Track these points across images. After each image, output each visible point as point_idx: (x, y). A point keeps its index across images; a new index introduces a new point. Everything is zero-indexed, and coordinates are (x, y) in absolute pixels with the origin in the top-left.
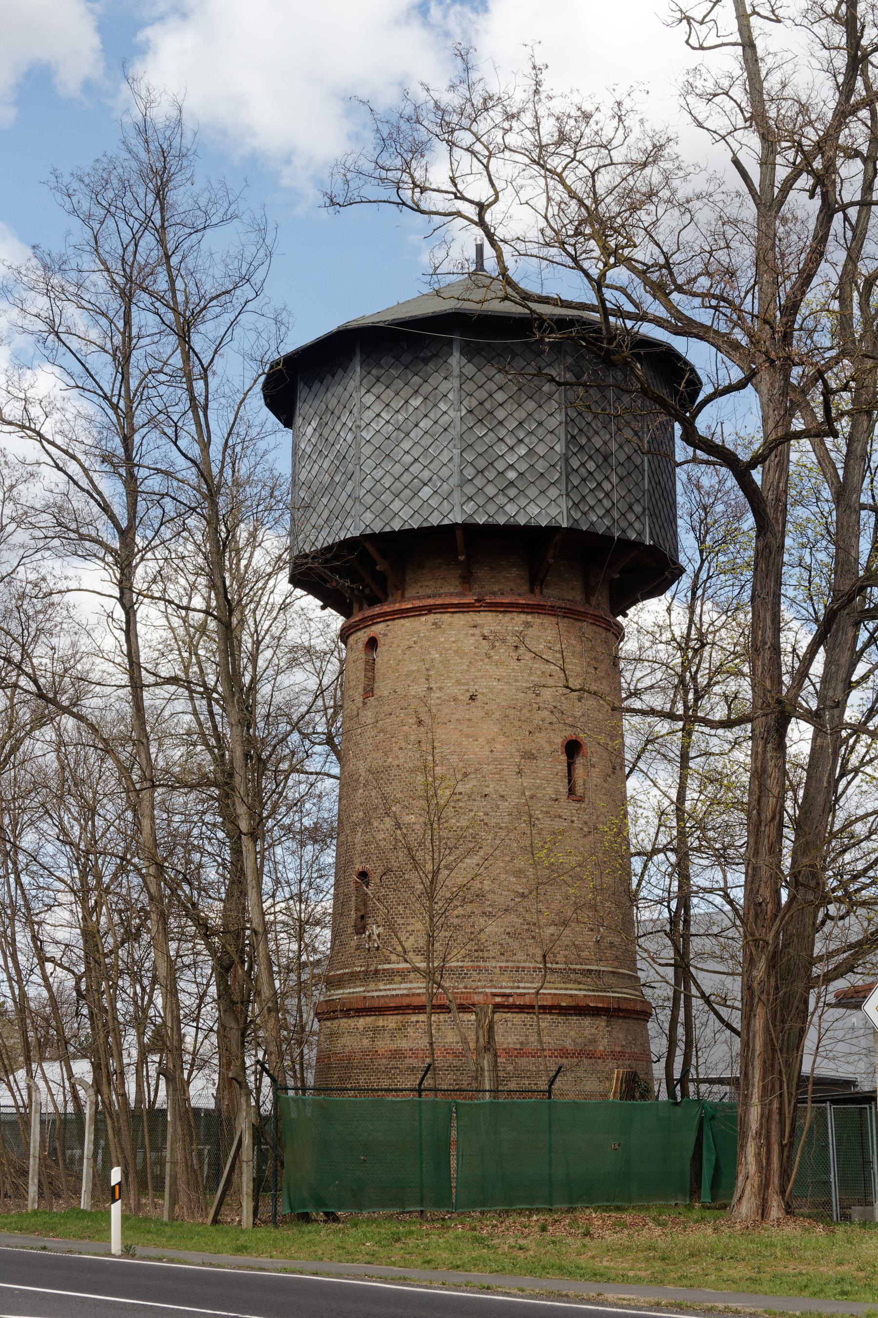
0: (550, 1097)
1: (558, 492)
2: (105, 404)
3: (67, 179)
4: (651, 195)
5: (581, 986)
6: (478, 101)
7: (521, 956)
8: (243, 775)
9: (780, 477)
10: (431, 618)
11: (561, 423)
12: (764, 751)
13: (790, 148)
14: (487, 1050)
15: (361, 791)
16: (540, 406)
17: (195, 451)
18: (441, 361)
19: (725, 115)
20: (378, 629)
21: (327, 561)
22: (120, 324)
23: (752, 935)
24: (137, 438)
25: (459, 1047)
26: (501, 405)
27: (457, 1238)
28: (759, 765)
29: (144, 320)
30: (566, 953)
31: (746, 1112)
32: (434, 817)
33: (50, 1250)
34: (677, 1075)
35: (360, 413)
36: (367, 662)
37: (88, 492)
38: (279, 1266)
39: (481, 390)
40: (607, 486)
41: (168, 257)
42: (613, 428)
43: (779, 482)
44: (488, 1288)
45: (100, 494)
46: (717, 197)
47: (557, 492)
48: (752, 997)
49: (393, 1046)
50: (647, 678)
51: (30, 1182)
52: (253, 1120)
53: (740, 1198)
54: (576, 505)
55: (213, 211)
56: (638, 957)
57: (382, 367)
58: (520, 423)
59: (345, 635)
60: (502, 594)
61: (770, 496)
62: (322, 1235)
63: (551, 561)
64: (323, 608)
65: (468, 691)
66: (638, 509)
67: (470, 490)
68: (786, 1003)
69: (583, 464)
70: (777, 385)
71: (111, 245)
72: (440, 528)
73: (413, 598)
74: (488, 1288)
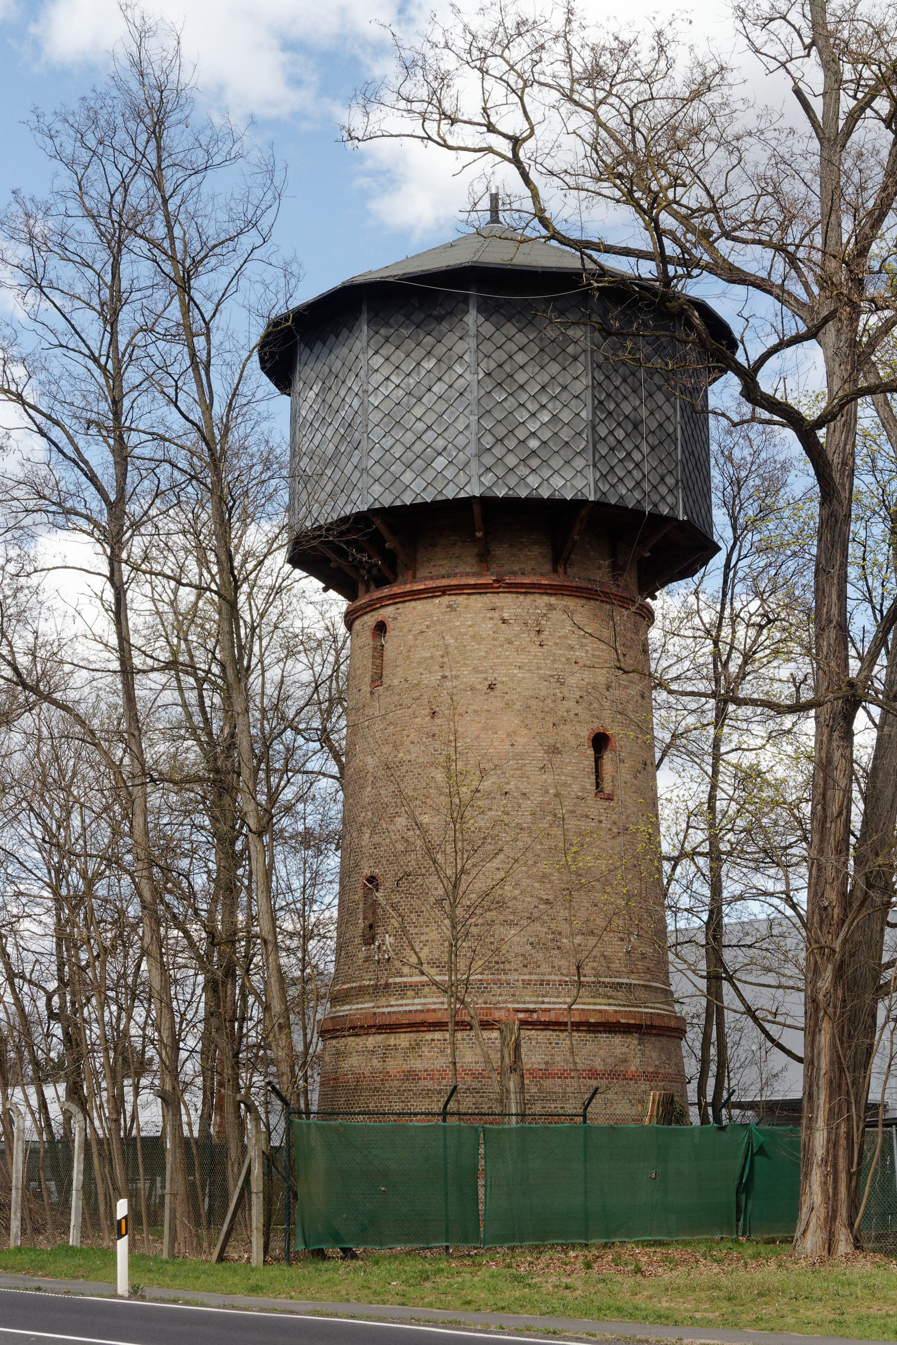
0: (585, 1122)
1: (585, 463)
2: (91, 364)
3: (49, 119)
4: (695, 133)
5: (611, 1001)
6: (510, 23)
7: (545, 968)
8: (232, 777)
9: (847, 438)
10: (446, 600)
11: (587, 387)
12: (830, 740)
13: (847, 82)
14: (513, 1070)
15: (369, 789)
16: (564, 369)
17: (196, 415)
18: (456, 319)
19: (785, 38)
20: (387, 613)
21: (341, 534)
22: (108, 278)
23: (817, 942)
24: (126, 403)
25: (480, 1067)
26: (521, 367)
27: (492, 1276)
28: (824, 755)
29: (138, 268)
30: (595, 964)
31: (810, 1137)
32: (457, 816)
33: (45, 1291)
34: (709, 1099)
35: (368, 377)
36: (375, 648)
37: (74, 461)
38: (310, 1308)
39: (500, 351)
40: (637, 456)
41: (165, 202)
42: (644, 394)
43: (845, 444)
44: (554, 1333)
45: (86, 463)
46: (769, 135)
47: (584, 463)
48: (817, 1009)
49: (406, 1067)
50: (675, 667)
51: (13, 1216)
52: (263, 1148)
53: (805, 1231)
54: (604, 476)
55: (216, 149)
56: (671, 969)
57: (391, 327)
58: (543, 387)
59: (350, 619)
60: (523, 574)
61: (836, 460)
62: (340, 1272)
63: (576, 537)
64: (325, 590)
65: (486, 679)
66: (670, 481)
67: (488, 460)
68: (853, 1020)
69: (611, 432)
70: (843, 337)
71: (98, 190)
72: (456, 501)
73: (426, 579)
74: (554, 1333)
